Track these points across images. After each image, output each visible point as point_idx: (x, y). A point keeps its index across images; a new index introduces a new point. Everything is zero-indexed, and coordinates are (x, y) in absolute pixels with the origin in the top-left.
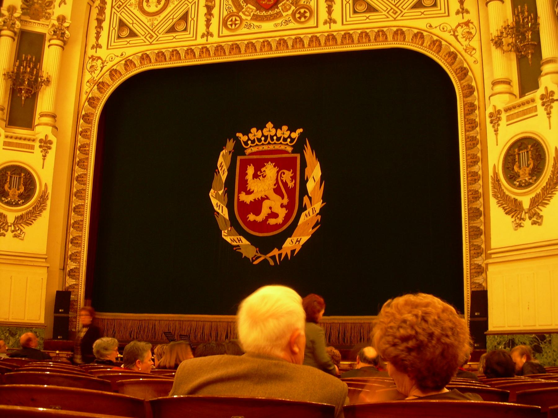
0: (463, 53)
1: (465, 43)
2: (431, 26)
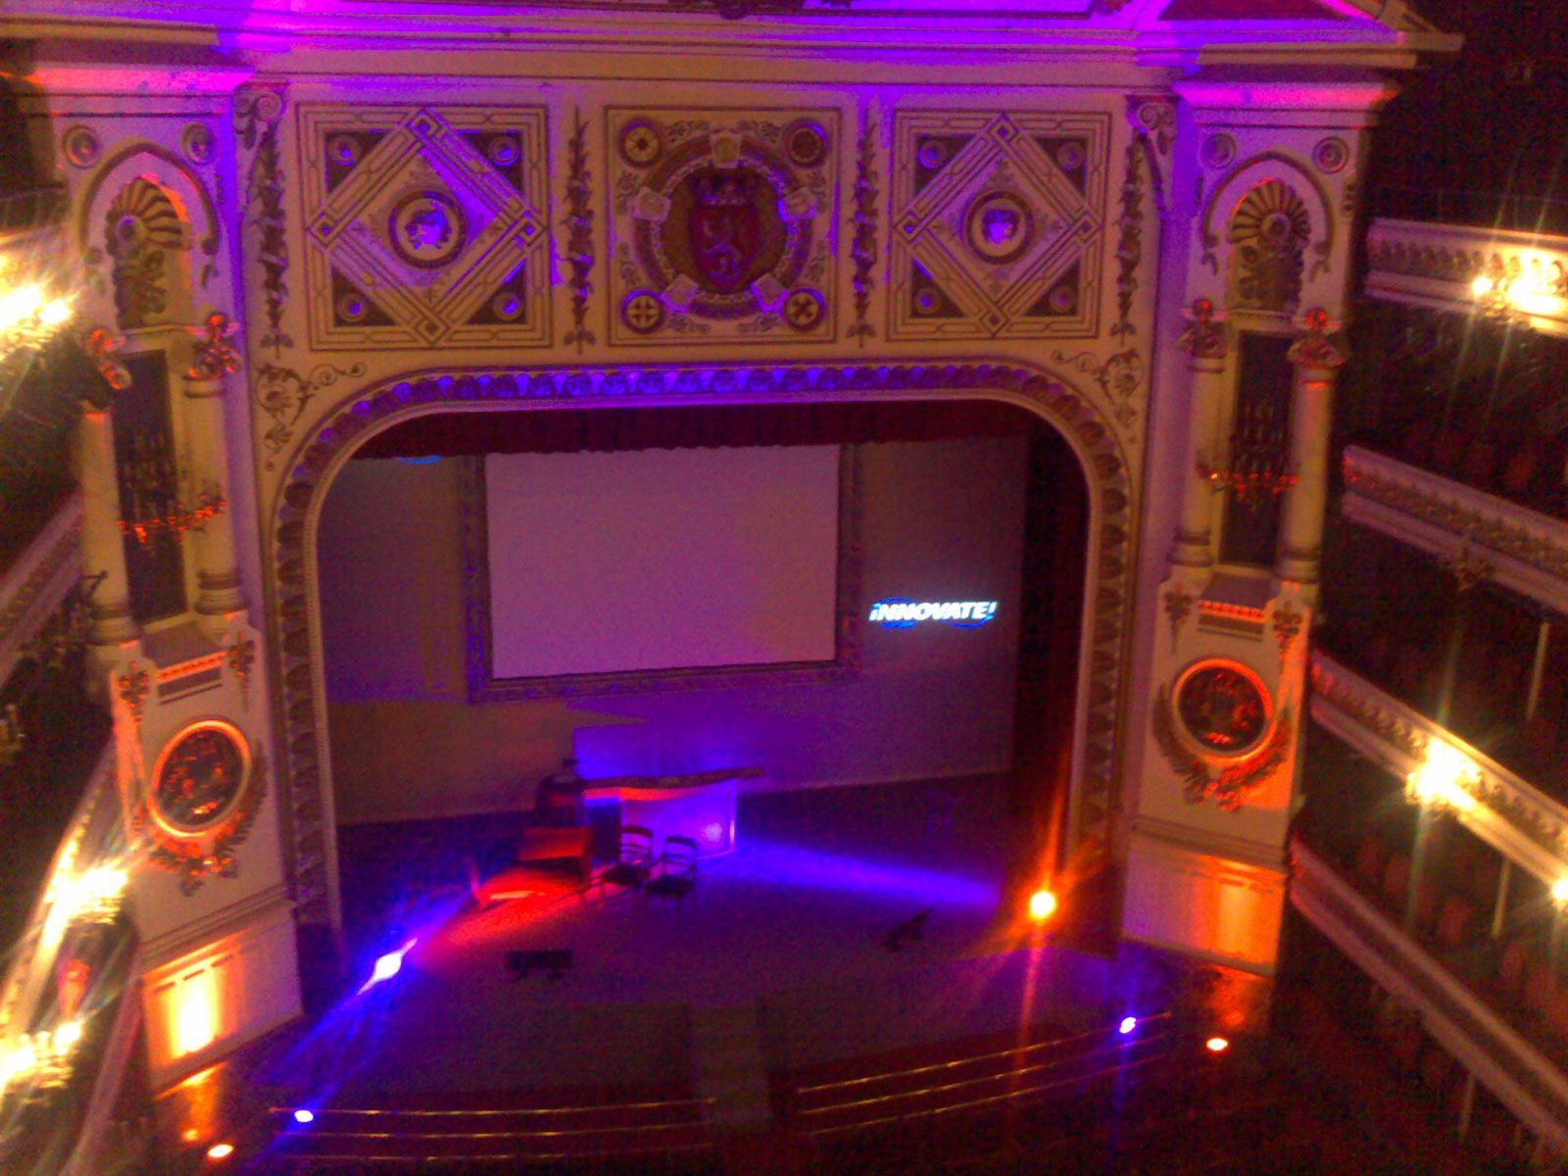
0: (1114, 421)
1: (1118, 400)
2: (1060, 358)
